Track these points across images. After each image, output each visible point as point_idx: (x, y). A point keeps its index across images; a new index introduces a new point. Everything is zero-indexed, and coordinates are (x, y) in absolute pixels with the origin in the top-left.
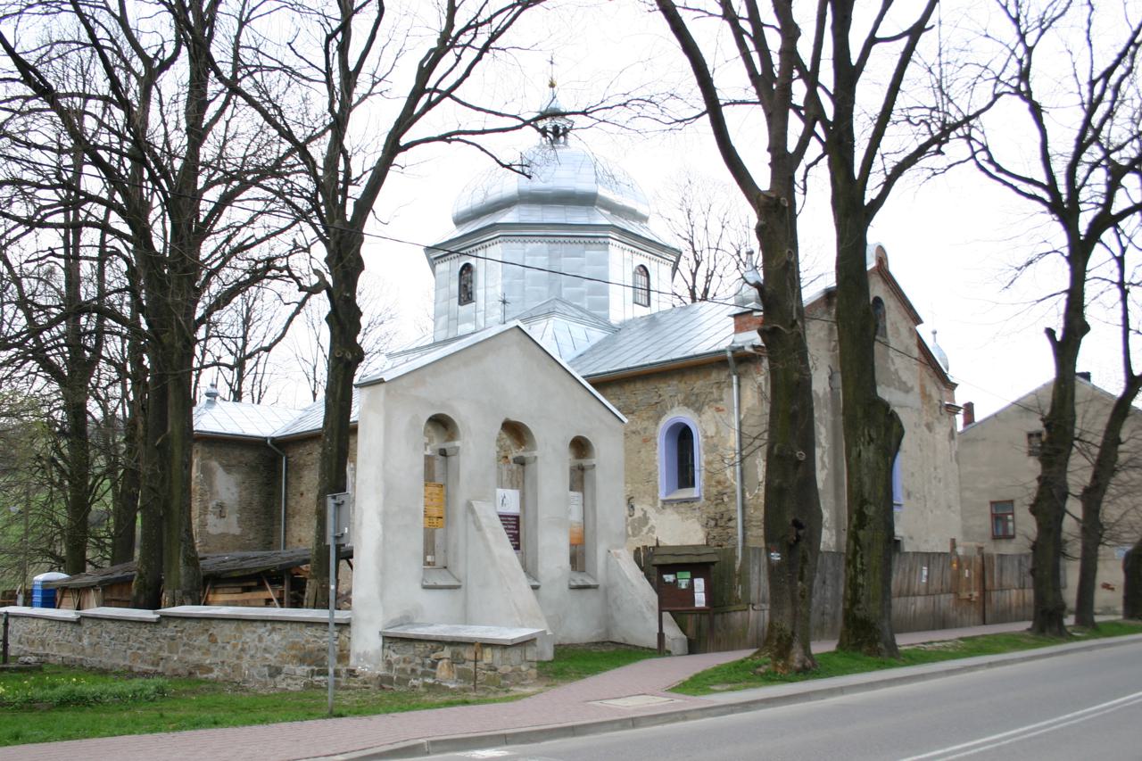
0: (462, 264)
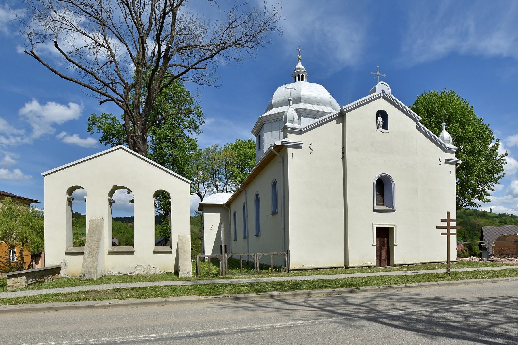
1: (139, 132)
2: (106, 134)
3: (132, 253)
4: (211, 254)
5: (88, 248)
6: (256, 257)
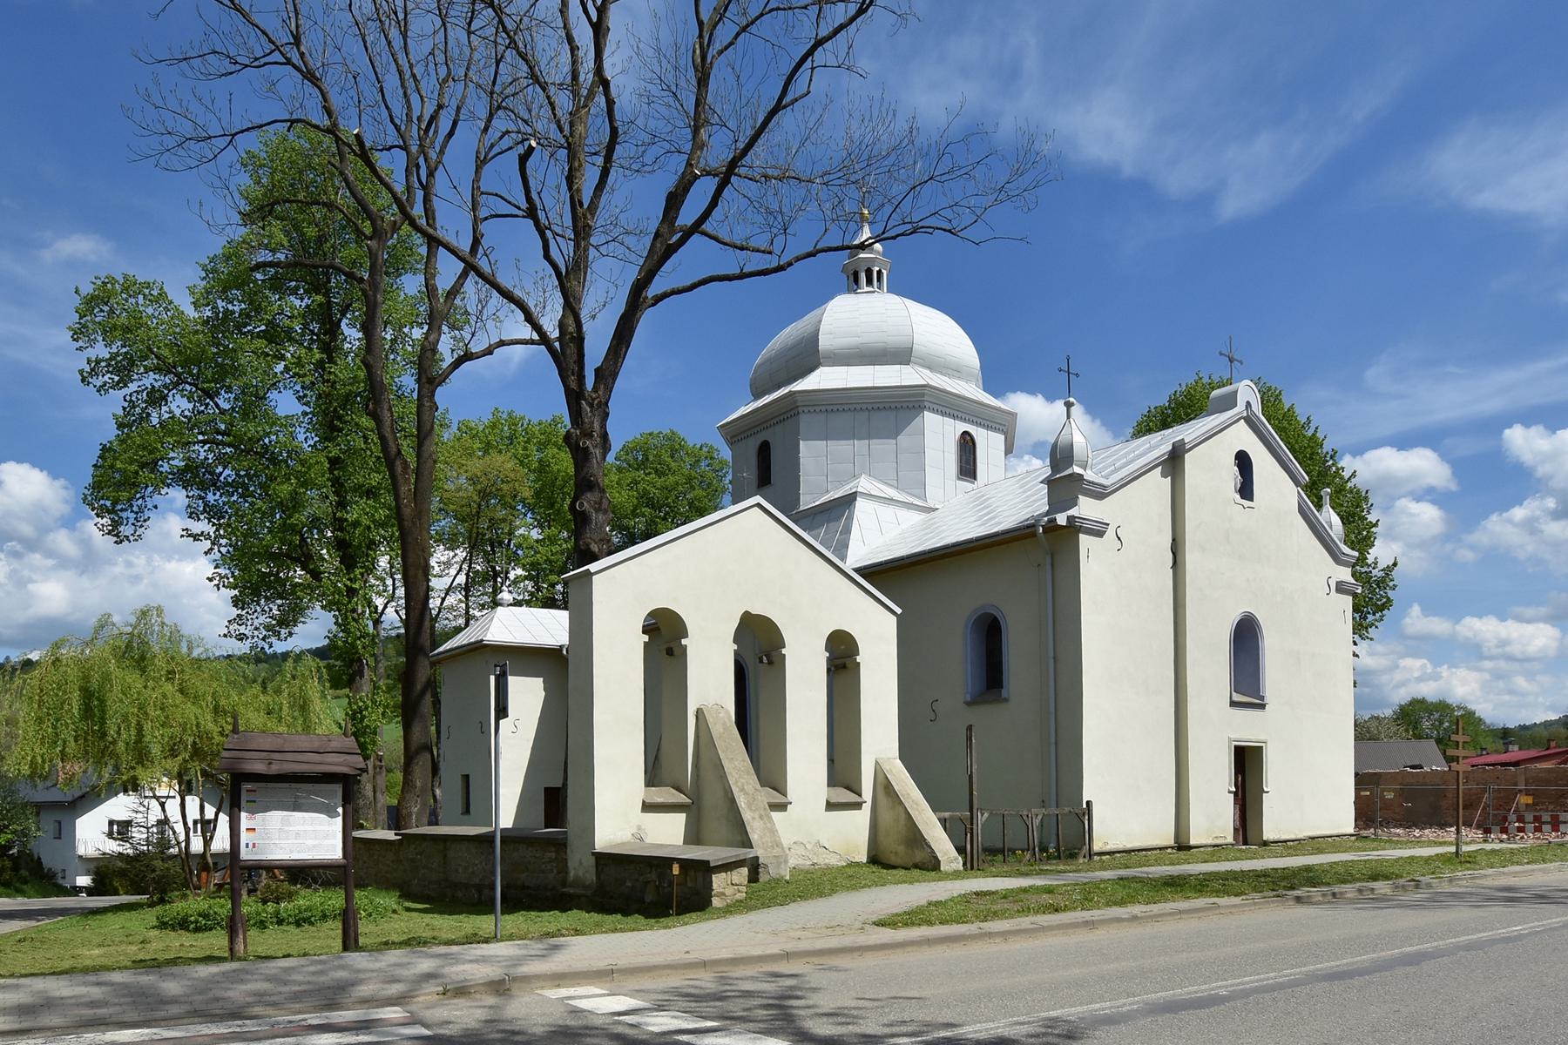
0: (759, 442)
6: (1030, 819)
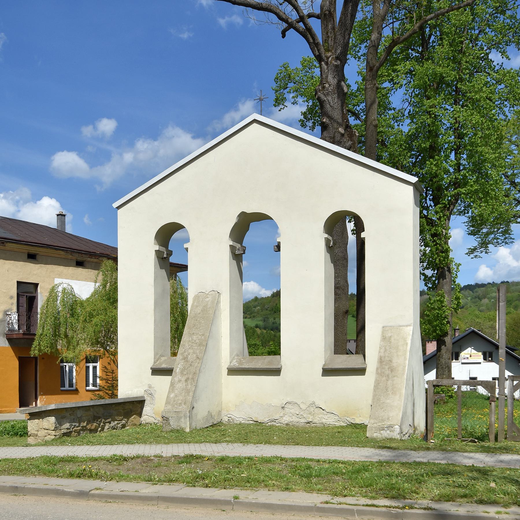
1: (330, 78)
2: (311, 104)
3: (276, 372)
4: (435, 378)
5: (182, 359)
